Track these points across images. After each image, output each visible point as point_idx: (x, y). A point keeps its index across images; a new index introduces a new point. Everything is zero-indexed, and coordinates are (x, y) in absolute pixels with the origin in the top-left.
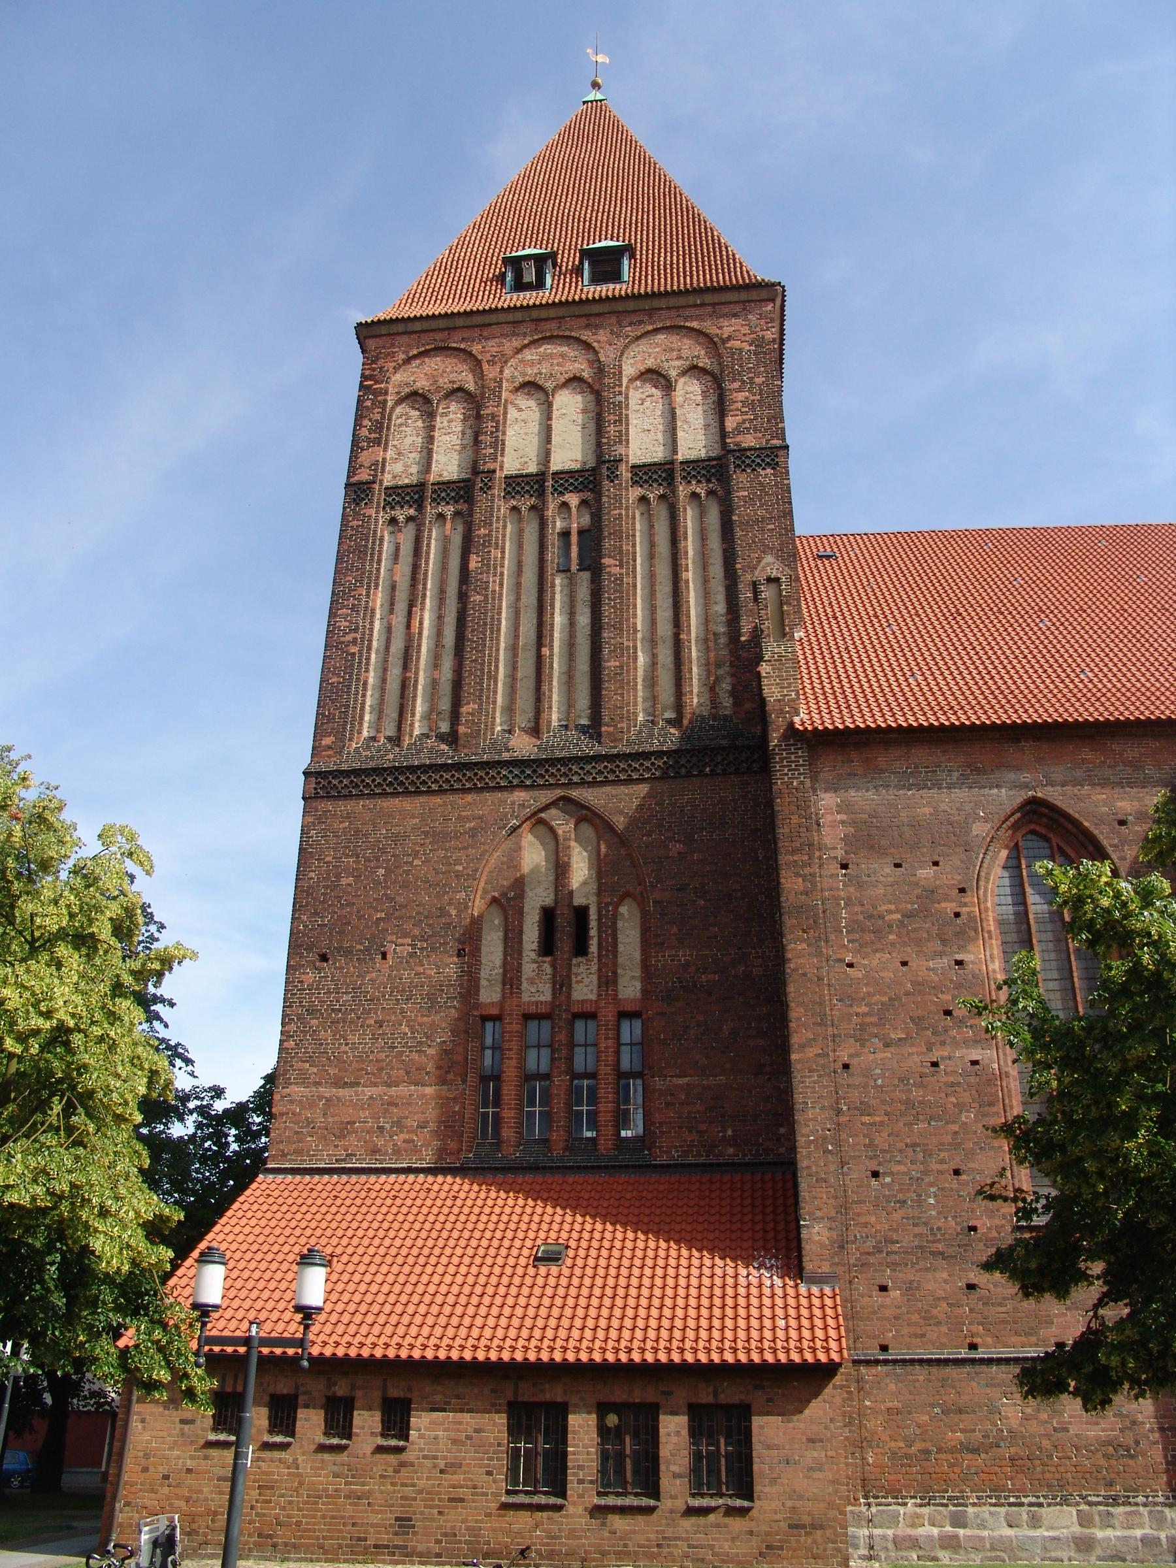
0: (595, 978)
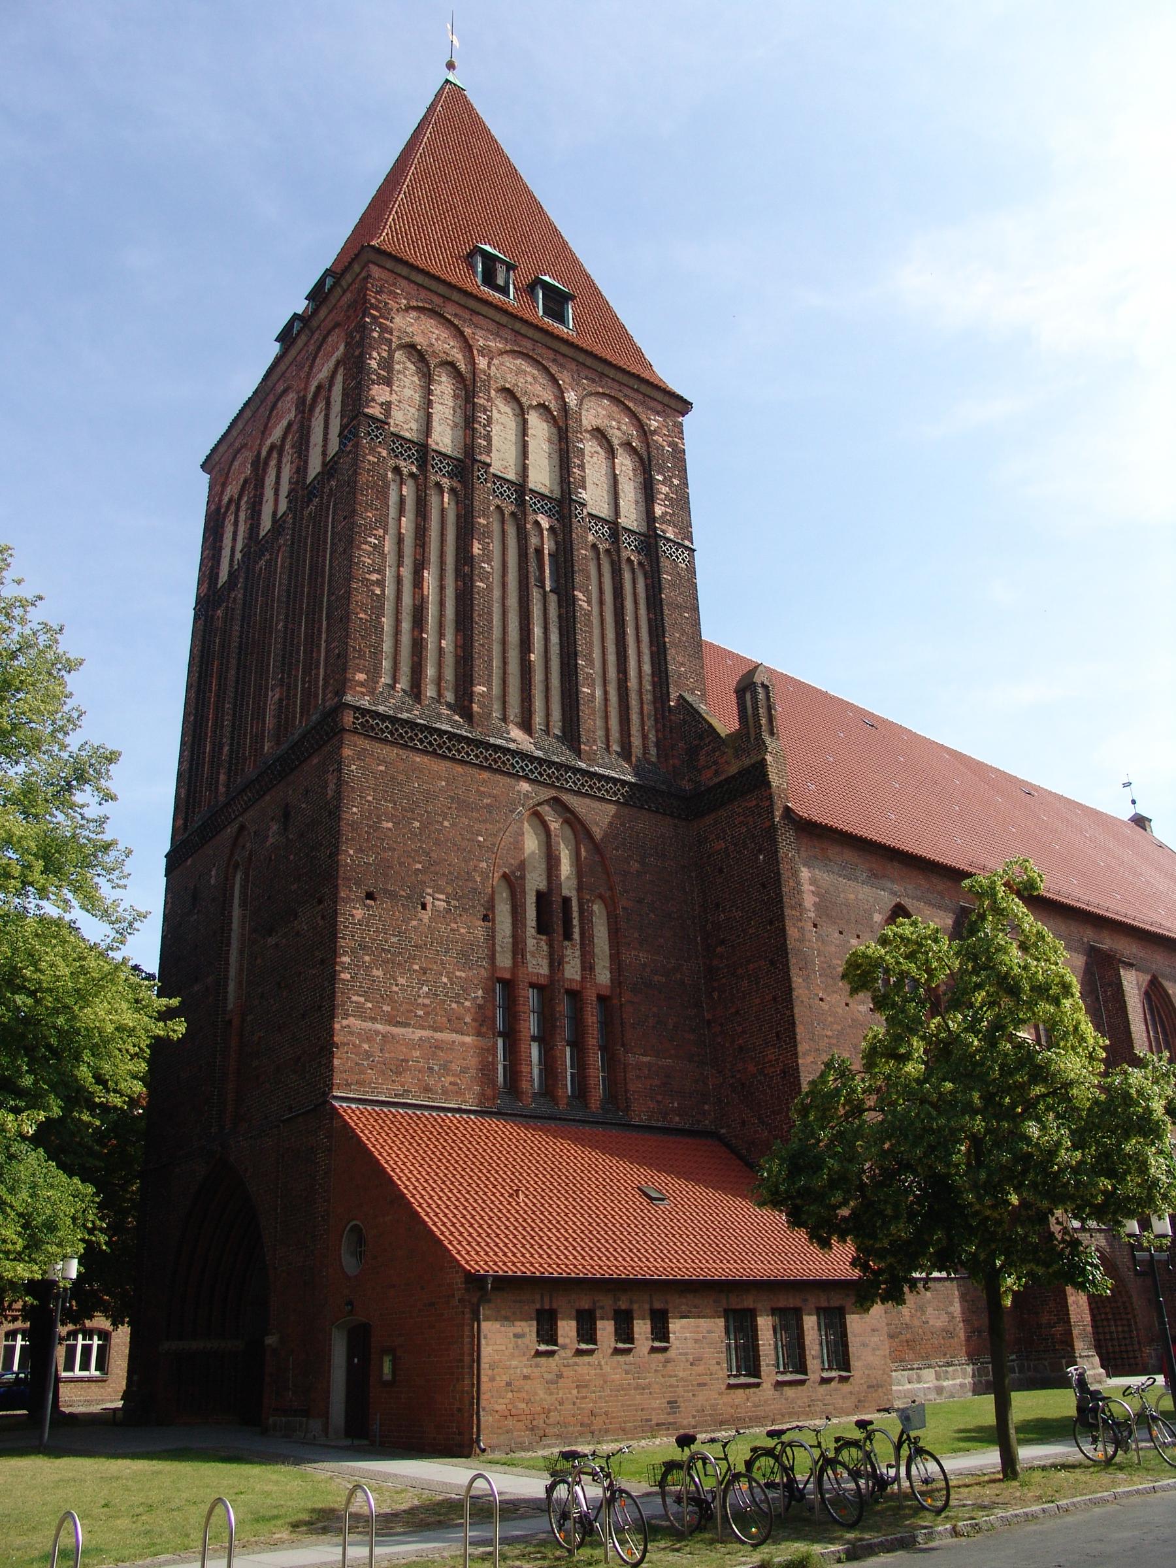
0: (578, 961)
